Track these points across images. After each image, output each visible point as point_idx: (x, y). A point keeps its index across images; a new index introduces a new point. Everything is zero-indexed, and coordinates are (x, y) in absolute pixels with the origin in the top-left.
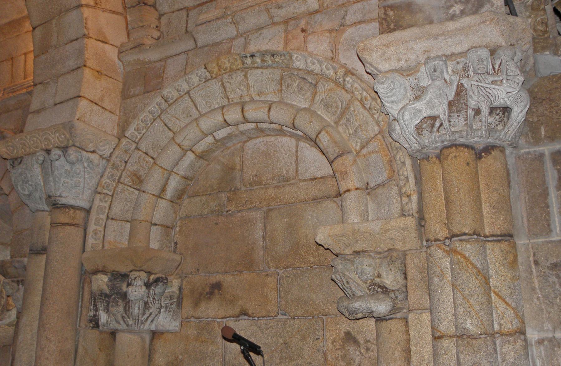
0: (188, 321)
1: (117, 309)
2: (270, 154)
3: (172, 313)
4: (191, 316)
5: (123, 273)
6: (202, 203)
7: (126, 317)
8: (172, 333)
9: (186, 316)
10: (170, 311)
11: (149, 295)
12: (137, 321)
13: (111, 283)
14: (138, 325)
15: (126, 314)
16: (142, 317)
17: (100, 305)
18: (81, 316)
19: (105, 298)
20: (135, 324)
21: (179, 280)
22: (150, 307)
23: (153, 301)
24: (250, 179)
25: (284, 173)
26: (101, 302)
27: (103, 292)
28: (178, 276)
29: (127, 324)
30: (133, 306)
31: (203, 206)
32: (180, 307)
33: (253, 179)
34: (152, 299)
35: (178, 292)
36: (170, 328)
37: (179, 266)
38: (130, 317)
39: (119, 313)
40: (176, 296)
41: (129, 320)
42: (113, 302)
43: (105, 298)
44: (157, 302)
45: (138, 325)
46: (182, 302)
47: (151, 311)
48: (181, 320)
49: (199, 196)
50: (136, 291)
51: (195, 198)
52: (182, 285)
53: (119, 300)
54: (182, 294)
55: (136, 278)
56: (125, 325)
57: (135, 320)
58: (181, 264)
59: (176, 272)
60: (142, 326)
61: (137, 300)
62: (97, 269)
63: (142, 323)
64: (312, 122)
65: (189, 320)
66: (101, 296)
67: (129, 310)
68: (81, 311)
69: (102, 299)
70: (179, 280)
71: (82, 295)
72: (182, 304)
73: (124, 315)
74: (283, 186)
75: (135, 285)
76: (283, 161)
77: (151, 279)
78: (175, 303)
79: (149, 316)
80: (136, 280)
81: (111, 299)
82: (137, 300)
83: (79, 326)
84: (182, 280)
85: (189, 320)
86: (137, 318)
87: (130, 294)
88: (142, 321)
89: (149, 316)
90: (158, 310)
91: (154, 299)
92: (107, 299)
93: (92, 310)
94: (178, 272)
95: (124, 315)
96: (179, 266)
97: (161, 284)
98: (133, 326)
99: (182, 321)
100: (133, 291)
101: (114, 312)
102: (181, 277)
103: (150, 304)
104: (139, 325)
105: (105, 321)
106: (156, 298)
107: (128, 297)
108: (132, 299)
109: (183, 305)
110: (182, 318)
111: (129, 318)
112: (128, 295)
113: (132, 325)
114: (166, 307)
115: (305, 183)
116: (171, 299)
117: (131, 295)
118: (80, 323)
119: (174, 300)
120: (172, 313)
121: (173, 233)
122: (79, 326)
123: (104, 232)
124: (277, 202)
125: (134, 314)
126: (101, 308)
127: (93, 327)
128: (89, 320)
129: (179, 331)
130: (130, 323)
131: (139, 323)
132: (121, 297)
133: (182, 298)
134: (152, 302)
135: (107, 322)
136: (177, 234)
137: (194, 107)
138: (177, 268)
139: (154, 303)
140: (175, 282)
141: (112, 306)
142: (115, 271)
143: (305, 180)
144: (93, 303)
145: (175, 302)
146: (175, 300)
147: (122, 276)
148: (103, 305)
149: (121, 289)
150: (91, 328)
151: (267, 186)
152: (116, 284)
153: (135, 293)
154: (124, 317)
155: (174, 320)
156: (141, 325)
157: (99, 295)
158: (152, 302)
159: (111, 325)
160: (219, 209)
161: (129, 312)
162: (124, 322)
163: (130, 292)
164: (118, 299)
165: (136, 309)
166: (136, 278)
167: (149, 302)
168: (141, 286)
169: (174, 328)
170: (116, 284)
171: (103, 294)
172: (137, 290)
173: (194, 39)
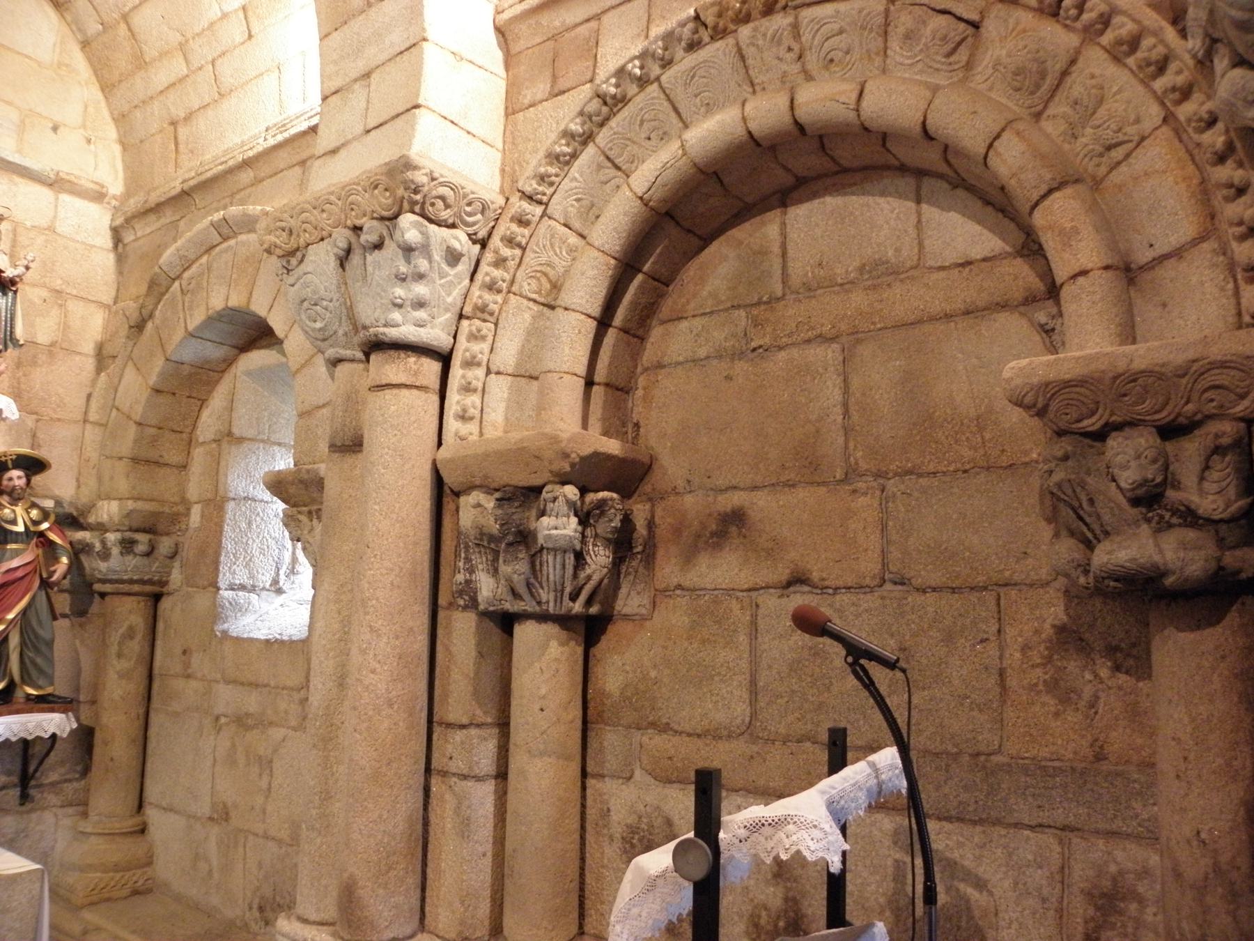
0: (670, 596)
2: (852, 213)
3: (631, 577)
4: (675, 584)
6: (694, 333)
10: (629, 574)
19: (489, 543)
21: (648, 506)
24: (806, 275)
25: (890, 254)
31: (696, 341)
33: (812, 273)
41: (541, 591)
49: (686, 318)
51: (676, 322)
52: (653, 517)
62: (471, 482)
64: (975, 112)
70: (648, 506)
73: (532, 580)
74: (889, 285)
76: (885, 226)
84: (653, 506)
95: (532, 580)
98: (551, 604)
102: (650, 500)
111: (542, 588)
115: (942, 274)
124: (874, 323)
137: (673, 114)
143: (942, 268)
148: (484, 559)
151: (847, 287)
155: (639, 593)
160: (733, 346)
168: (591, 81)
171: (485, 534)
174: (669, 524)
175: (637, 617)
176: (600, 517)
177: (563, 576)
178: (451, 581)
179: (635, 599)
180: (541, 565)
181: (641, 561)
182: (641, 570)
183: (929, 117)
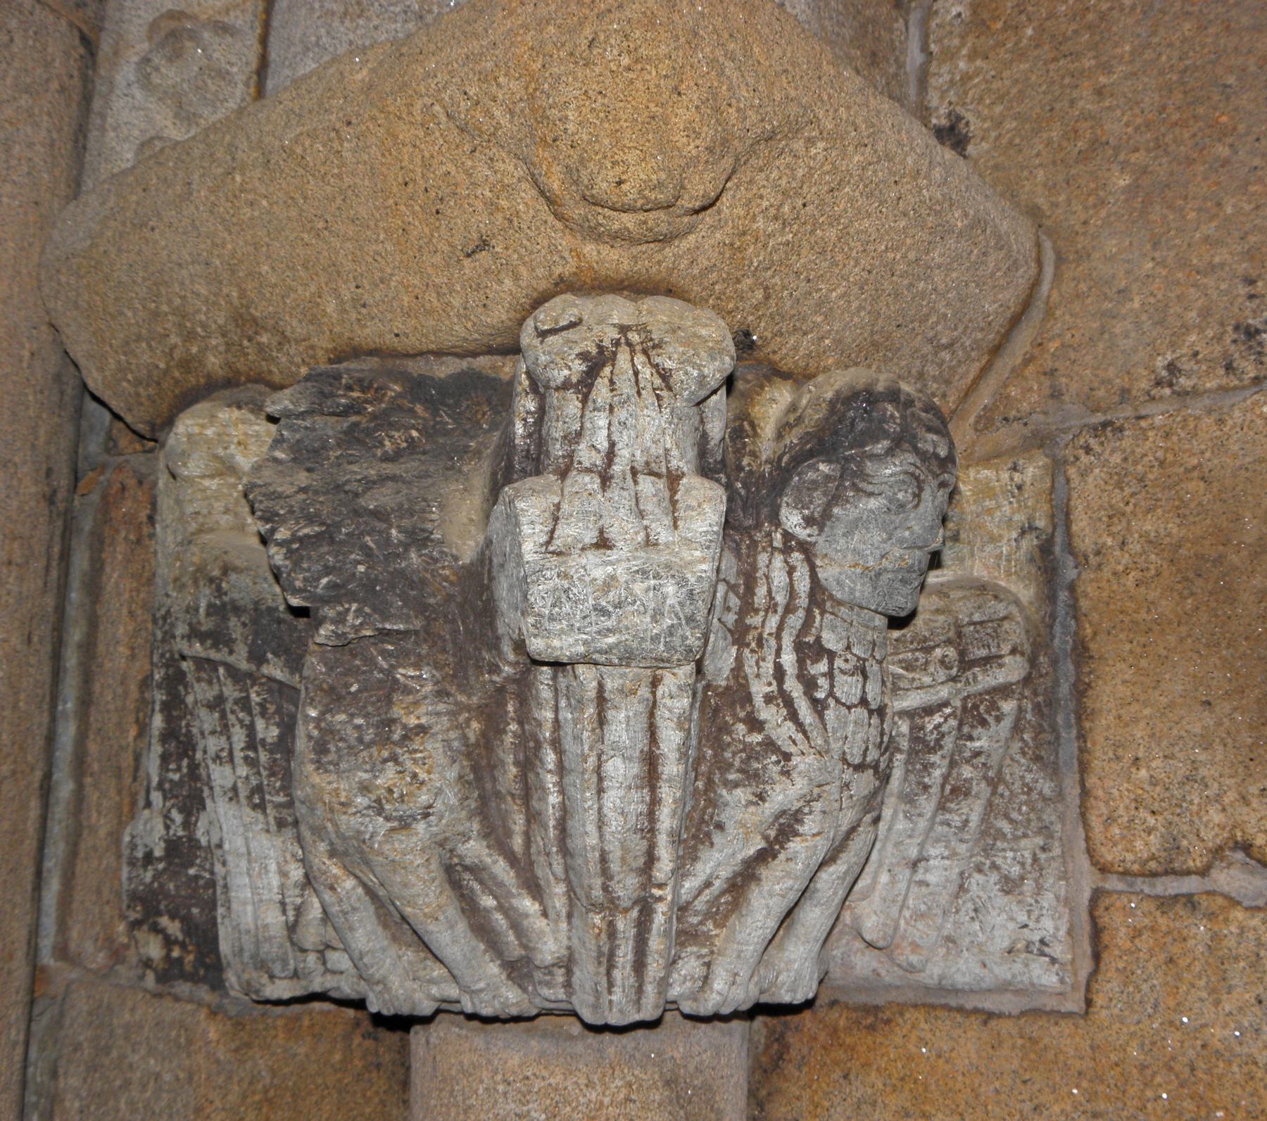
0: (1190, 901)
1: (388, 776)
3: (973, 810)
4: (1212, 837)
5: (445, 369)
7: (500, 868)
8: (989, 1016)
9: (1147, 846)
10: (960, 791)
11: (748, 607)
12: (625, 925)
13: (303, 478)
14: (639, 966)
15: (496, 836)
16: (680, 872)
17: (213, 744)
18: (73, 853)
19: (257, 657)
20: (609, 961)
21: (1033, 470)
22: (770, 745)
23: (809, 685)
26: (217, 704)
27: (241, 588)
28: (1005, 436)
29: (516, 951)
30: (580, 742)
32: (1069, 749)
34: (788, 659)
35: (1025, 592)
36: (964, 970)
37: (1015, 322)
38: (550, 870)
39: (405, 824)
40: (1015, 632)
41: (528, 904)
42: (335, 698)
43: (257, 657)
44: (848, 688)
45: (639, 966)
46: (1081, 690)
47: (783, 795)
48: (1088, 881)
50: (603, 543)
52: (1062, 515)
53: (404, 673)
54: (1074, 608)
55: (597, 362)
56: (494, 969)
57: (611, 905)
58: (1036, 314)
59: (985, 397)
60: (690, 966)
61: (627, 658)
62: (186, 364)
63: (686, 936)
65: (1190, 885)
66: (218, 638)
67: (528, 792)
68: (79, 797)
69: (233, 672)
70: (1033, 470)
71: (88, 648)
72: (1082, 714)
73: (475, 849)
75: (585, 455)
77: (768, 430)
78: (1008, 706)
79: (765, 856)
80: (601, 391)
81: (314, 665)
82: (627, 658)
83: (62, 952)
84: (1057, 467)
85: (1190, 885)
86: (626, 886)
87: (523, 583)
88: (683, 909)
89: (765, 856)
90: (864, 783)
91: (809, 650)
92: (275, 670)
93: (156, 797)
94: (1002, 398)
95: (475, 849)
96: (1015, 322)
97: (889, 470)
98: (586, 973)
99: (1097, 895)
100: (567, 532)
101: (348, 822)
102: (1040, 441)
103: (770, 714)
104: (654, 969)
105: (274, 919)
106: (831, 641)
107: (508, 621)
108: (565, 645)
109: (1103, 727)
110: (1104, 869)
111: (535, 889)
112: (503, 590)
113: (568, 963)
114: (921, 746)
116: (966, 664)
117: (540, 595)
118: (63, 926)
119: (999, 676)
120: (973, 810)
121: (914, 56)
122: (62, 952)
123: (264, 41)
125: (587, 837)
126: (221, 776)
127: (169, 972)
128: (134, 897)
129: (1074, 1004)
130: (549, 948)
131: (655, 943)
132: (428, 634)
133: (1081, 652)
134: (794, 687)
135: (292, 928)
136: (950, 55)
138: (996, 350)
139: (819, 707)
140: (985, 491)
141: (321, 748)
142: (357, 352)
144: (158, 721)
145: (1004, 691)
146: (1011, 670)
147: (433, 406)
148: (239, 736)
149: (418, 538)
150: (150, 979)
152: (369, 484)
153: (596, 567)
154: (476, 870)
155: (1010, 886)
156: (672, 963)
157: (195, 633)
158: (794, 687)
159: (338, 959)
161: (533, 817)
162: (481, 928)
163: (529, 549)
164: (402, 657)
165: (620, 770)
166: (597, 362)
167: (759, 689)
168: (673, 479)
169: (1003, 972)
170: (369, 484)
171: (237, 610)
172: (623, 527)
173: (531, 1019)
174: (1152, 542)
175: (1008, 1004)
176: (836, 498)
177: (650, 831)
178: (115, 837)
179: (996, 919)
180: (528, 764)
181: (1017, 729)
182: (1020, 771)
183: (437, 1031)
